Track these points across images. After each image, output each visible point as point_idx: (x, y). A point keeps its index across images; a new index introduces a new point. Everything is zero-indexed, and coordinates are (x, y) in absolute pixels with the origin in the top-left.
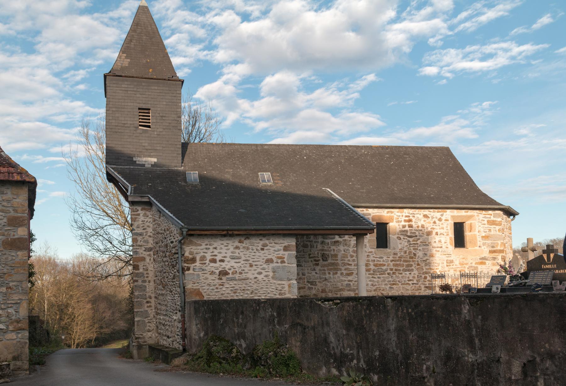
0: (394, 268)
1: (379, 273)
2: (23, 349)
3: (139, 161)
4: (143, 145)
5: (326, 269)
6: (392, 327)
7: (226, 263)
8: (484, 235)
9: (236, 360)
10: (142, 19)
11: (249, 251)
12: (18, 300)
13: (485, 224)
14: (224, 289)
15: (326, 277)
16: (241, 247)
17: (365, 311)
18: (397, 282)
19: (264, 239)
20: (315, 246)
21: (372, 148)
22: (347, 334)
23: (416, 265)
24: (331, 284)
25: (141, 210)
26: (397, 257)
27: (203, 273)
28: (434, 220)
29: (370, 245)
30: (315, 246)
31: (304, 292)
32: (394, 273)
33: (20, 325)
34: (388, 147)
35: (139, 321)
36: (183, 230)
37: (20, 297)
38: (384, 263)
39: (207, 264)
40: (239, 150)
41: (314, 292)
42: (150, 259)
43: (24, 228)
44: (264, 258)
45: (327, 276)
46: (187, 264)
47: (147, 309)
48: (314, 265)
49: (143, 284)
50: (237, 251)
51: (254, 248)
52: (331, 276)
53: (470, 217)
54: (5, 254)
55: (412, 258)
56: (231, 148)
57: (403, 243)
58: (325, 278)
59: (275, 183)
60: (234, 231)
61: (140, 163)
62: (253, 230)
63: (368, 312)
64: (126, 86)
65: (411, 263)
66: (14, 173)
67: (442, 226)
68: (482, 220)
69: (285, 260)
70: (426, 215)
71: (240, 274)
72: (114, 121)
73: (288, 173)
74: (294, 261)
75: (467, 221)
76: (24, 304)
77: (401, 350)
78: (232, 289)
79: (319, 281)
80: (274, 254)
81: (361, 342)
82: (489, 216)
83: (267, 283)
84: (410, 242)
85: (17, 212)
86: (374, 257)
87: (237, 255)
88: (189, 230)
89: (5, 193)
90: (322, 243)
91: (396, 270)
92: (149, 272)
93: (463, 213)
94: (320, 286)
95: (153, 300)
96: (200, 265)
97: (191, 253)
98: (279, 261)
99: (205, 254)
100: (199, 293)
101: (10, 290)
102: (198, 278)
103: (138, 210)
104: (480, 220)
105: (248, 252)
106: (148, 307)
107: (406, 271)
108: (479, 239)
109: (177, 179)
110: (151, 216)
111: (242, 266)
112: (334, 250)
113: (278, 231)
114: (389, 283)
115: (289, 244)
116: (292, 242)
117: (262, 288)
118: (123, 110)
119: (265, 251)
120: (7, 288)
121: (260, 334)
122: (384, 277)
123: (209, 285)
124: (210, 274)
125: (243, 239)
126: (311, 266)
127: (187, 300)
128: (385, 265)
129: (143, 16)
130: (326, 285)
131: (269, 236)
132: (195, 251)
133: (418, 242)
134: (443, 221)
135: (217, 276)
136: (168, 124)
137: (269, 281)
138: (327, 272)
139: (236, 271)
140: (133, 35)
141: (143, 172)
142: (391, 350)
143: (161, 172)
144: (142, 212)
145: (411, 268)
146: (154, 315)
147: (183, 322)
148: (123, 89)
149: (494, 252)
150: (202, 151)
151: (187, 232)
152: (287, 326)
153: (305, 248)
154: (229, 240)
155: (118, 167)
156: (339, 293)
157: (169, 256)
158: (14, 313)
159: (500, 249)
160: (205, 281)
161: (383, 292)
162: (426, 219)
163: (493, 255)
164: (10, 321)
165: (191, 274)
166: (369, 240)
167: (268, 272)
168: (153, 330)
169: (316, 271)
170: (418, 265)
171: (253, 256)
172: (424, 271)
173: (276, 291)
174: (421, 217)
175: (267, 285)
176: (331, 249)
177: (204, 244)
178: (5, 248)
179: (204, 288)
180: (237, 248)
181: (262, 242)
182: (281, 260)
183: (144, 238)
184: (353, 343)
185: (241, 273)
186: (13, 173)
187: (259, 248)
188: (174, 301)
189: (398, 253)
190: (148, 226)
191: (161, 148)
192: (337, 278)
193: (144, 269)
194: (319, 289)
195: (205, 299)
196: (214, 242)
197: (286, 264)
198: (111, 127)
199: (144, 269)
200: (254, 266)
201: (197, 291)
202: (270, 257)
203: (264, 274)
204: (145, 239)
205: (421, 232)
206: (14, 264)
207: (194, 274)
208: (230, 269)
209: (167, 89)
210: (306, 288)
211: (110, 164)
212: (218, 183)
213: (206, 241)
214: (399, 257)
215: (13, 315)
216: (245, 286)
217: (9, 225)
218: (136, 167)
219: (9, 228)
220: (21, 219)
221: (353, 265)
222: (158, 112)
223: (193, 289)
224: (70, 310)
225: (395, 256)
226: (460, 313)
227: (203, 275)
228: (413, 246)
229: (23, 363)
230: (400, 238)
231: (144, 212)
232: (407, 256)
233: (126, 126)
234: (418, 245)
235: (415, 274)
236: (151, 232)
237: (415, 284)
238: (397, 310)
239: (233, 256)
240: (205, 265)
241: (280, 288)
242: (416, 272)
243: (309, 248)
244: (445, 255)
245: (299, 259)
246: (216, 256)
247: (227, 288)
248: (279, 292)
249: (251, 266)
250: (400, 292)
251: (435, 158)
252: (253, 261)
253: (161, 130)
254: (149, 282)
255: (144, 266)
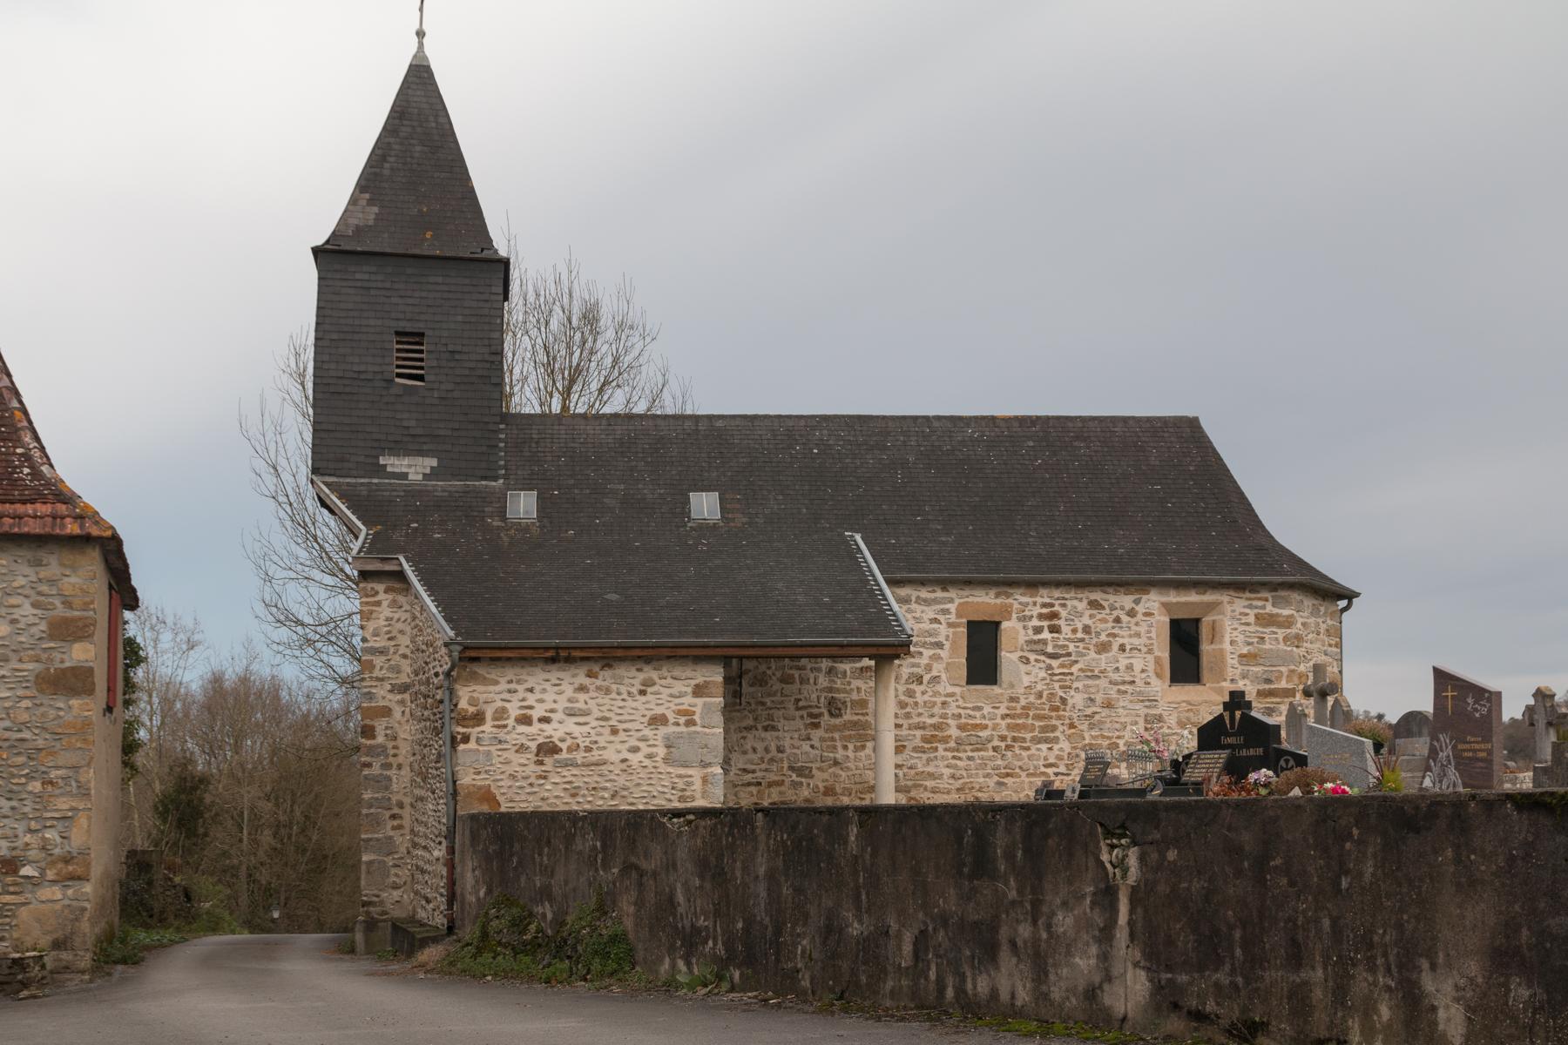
0: (1010, 735)
1: (971, 747)
2: (77, 924)
3: (392, 465)
4: (405, 424)
5: (838, 738)
6: (762, 871)
7: (554, 725)
8: (1245, 650)
9: (533, 947)
10: (415, 99)
11: (611, 696)
12: (69, 810)
13: (1248, 624)
14: (548, 787)
15: (838, 756)
16: (592, 688)
17: (727, 837)
18: (1017, 770)
19: (646, 668)
20: (812, 681)
21: (994, 423)
22: (701, 887)
23: (1065, 728)
24: (850, 773)
25: (385, 592)
26: (1018, 706)
27: (500, 750)
28: (1115, 613)
29: (949, 679)
30: (812, 681)
31: (780, 793)
32: (1008, 747)
33: (70, 868)
34: (1038, 418)
35: (370, 863)
36: (452, 647)
37: (73, 804)
38: (984, 722)
39: (509, 728)
40: (650, 432)
41: (805, 793)
42: (403, 712)
43: (88, 644)
44: (646, 713)
45: (840, 754)
46: (464, 726)
47: (391, 833)
48: (806, 726)
49: (385, 773)
50: (582, 697)
51: (623, 689)
52: (850, 753)
53: (1211, 607)
54: (41, 705)
55: (1056, 709)
56: (630, 428)
57: (1035, 671)
58: (835, 758)
59: (727, 519)
60: (571, 651)
61: (397, 470)
62: (617, 648)
63: (730, 839)
64: (366, 277)
65: (1054, 722)
66: (68, 516)
67: (1138, 629)
68: (1241, 614)
69: (697, 718)
70: (1096, 601)
71: (586, 751)
72: (333, 366)
73: (765, 493)
74: (718, 719)
75: (1205, 616)
76: (82, 820)
77: (771, 916)
78: (568, 786)
79: (818, 765)
80: (671, 705)
81: (719, 904)
82: (1260, 603)
83: (652, 773)
84: (1053, 669)
85: (72, 608)
86: (958, 707)
87: (581, 705)
88: (466, 648)
89: (44, 563)
90: (830, 671)
91: (1014, 739)
92: (400, 743)
93: (1193, 597)
94: (820, 779)
95: (407, 812)
96: (494, 730)
97: (473, 702)
98: (682, 720)
99: (507, 705)
100: (488, 796)
101: (50, 788)
102: (488, 761)
103: (377, 593)
104: (1237, 613)
105: (606, 700)
106: (394, 828)
107: (1039, 743)
108: (1231, 660)
109: (484, 511)
110: (409, 608)
111: (593, 732)
112: (859, 689)
113: (678, 650)
114: (996, 772)
115: (708, 679)
116: (715, 675)
117: (638, 785)
118: (356, 337)
119: (649, 697)
120: (43, 783)
121: (574, 890)
122: (982, 758)
123: (512, 777)
124: (517, 751)
125: (596, 668)
126: (799, 730)
127: (460, 813)
128: (986, 727)
129: (419, 93)
130: (836, 776)
131: (658, 660)
132: (483, 697)
133: (1074, 669)
134: (1140, 617)
135: (532, 756)
136: (467, 372)
137: (655, 767)
138: (839, 744)
139: (578, 745)
140: (389, 143)
141: (402, 494)
142: (759, 918)
143: (446, 494)
144: (387, 596)
145: (1052, 735)
146: (407, 848)
147: (451, 865)
148: (359, 284)
149: (1271, 693)
150: (556, 436)
151: (460, 653)
152: (615, 871)
153: (788, 683)
154: (564, 670)
155: (341, 480)
156: (868, 797)
157: (432, 706)
158: (59, 840)
159: (1285, 686)
160: (504, 768)
161: (980, 795)
162: (1095, 612)
163: (1268, 703)
164: (49, 859)
165: (470, 750)
166: (948, 664)
167: (655, 746)
168: (405, 883)
169: (813, 743)
170: (1072, 726)
171: (620, 708)
172: (1087, 742)
173: (673, 792)
174: (1081, 606)
175: (650, 778)
176: (852, 686)
177: (503, 681)
178: (41, 691)
179: (500, 784)
180: (582, 689)
181: (641, 676)
182: (686, 718)
183: (389, 660)
184: (708, 904)
185: (588, 749)
186: (63, 518)
187: (634, 690)
188: (438, 814)
189: (1022, 698)
190: (401, 632)
191: (449, 433)
192: (864, 758)
193: (386, 735)
194: (817, 787)
195: (503, 809)
196: (528, 674)
197: (698, 729)
198: (325, 381)
199: (386, 735)
200: (622, 734)
201: (483, 791)
202: (659, 711)
203: (645, 750)
204: (392, 662)
205: (1081, 645)
206: (60, 727)
207: (478, 750)
208: (563, 740)
209: (467, 281)
210: (786, 784)
211: (322, 475)
212: (582, 520)
213: (511, 673)
214: (1023, 708)
215: (56, 846)
216: (599, 779)
217: (52, 637)
218: (387, 481)
219: (52, 645)
220: (80, 624)
221: (905, 726)
222: (443, 341)
223: (474, 785)
224: (314, 838)
225: (1014, 704)
226: (846, 842)
227: (500, 753)
228: (1058, 681)
229: (76, 955)
230: (1028, 659)
231: (390, 597)
232: (1044, 704)
233: (362, 376)
234: (1073, 678)
235: (1061, 749)
236: (407, 647)
237: (1063, 774)
238: (769, 836)
239: (572, 708)
240: (505, 730)
241: (681, 786)
242: (1065, 745)
243: (797, 685)
244: (1142, 701)
245: (771, 712)
246: (531, 707)
247: (557, 784)
248: (680, 794)
249: (614, 732)
250: (1022, 795)
251: (1155, 448)
252: (620, 721)
253: (451, 387)
254: (400, 767)
255: (387, 728)
